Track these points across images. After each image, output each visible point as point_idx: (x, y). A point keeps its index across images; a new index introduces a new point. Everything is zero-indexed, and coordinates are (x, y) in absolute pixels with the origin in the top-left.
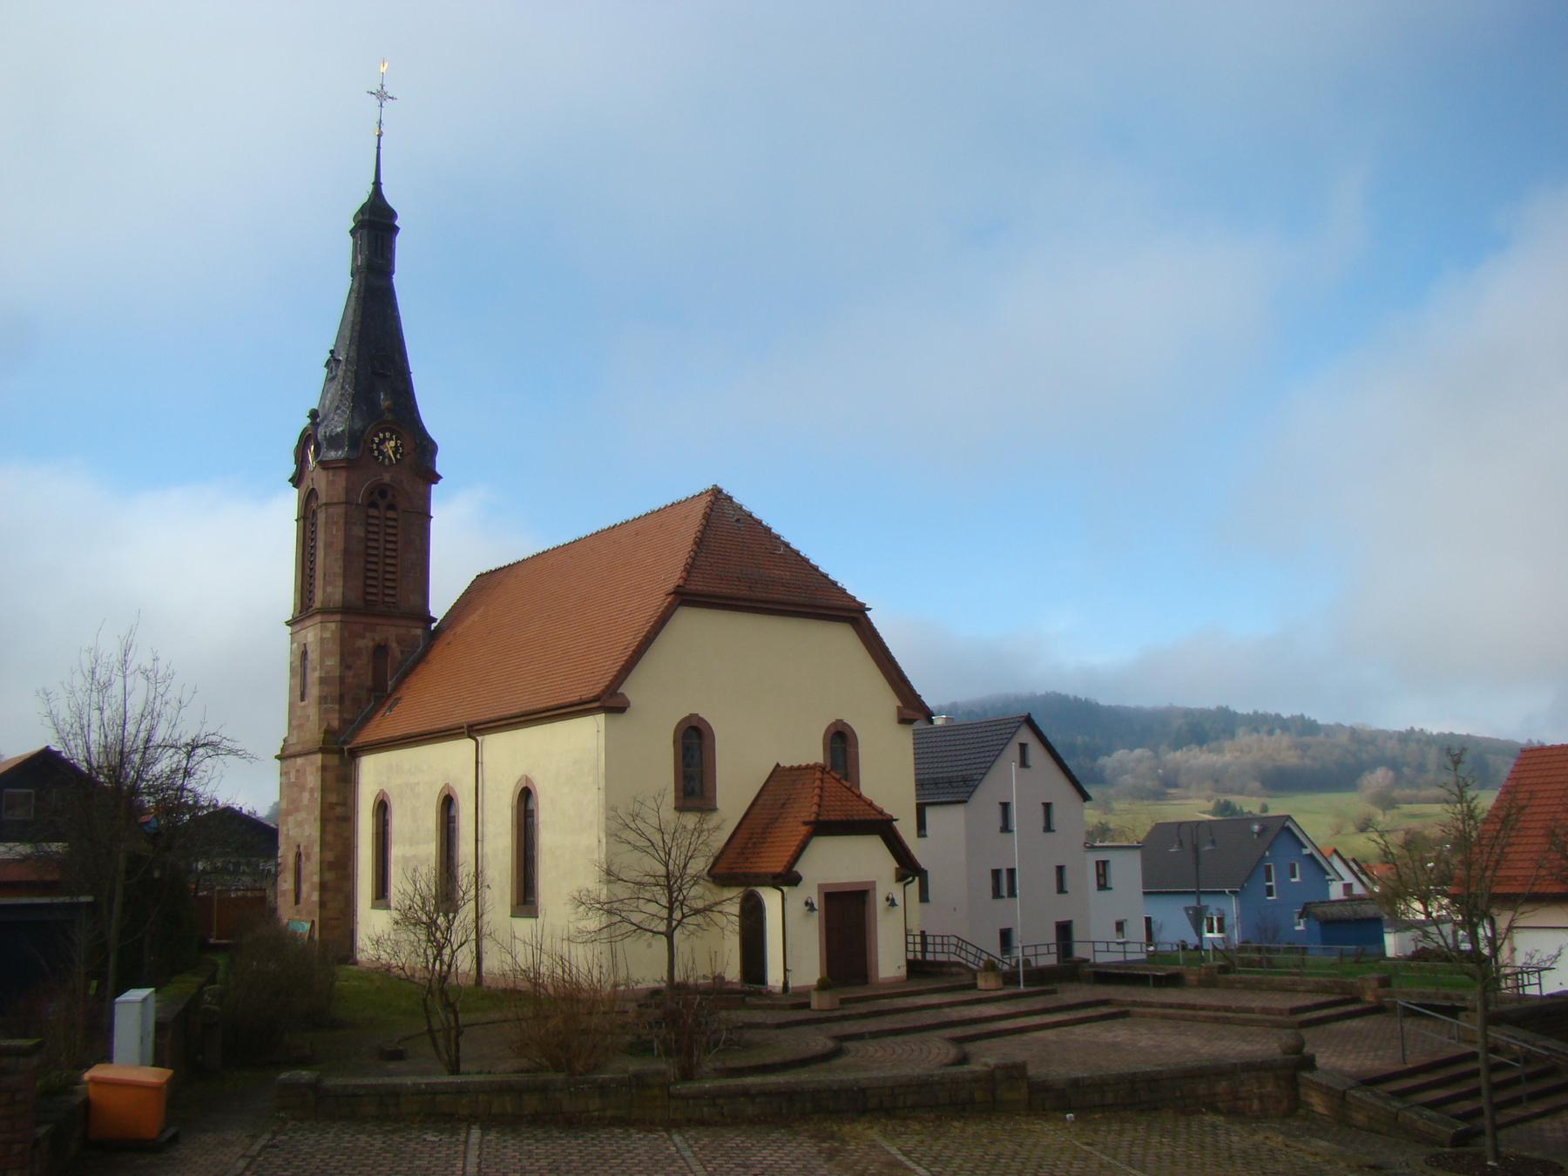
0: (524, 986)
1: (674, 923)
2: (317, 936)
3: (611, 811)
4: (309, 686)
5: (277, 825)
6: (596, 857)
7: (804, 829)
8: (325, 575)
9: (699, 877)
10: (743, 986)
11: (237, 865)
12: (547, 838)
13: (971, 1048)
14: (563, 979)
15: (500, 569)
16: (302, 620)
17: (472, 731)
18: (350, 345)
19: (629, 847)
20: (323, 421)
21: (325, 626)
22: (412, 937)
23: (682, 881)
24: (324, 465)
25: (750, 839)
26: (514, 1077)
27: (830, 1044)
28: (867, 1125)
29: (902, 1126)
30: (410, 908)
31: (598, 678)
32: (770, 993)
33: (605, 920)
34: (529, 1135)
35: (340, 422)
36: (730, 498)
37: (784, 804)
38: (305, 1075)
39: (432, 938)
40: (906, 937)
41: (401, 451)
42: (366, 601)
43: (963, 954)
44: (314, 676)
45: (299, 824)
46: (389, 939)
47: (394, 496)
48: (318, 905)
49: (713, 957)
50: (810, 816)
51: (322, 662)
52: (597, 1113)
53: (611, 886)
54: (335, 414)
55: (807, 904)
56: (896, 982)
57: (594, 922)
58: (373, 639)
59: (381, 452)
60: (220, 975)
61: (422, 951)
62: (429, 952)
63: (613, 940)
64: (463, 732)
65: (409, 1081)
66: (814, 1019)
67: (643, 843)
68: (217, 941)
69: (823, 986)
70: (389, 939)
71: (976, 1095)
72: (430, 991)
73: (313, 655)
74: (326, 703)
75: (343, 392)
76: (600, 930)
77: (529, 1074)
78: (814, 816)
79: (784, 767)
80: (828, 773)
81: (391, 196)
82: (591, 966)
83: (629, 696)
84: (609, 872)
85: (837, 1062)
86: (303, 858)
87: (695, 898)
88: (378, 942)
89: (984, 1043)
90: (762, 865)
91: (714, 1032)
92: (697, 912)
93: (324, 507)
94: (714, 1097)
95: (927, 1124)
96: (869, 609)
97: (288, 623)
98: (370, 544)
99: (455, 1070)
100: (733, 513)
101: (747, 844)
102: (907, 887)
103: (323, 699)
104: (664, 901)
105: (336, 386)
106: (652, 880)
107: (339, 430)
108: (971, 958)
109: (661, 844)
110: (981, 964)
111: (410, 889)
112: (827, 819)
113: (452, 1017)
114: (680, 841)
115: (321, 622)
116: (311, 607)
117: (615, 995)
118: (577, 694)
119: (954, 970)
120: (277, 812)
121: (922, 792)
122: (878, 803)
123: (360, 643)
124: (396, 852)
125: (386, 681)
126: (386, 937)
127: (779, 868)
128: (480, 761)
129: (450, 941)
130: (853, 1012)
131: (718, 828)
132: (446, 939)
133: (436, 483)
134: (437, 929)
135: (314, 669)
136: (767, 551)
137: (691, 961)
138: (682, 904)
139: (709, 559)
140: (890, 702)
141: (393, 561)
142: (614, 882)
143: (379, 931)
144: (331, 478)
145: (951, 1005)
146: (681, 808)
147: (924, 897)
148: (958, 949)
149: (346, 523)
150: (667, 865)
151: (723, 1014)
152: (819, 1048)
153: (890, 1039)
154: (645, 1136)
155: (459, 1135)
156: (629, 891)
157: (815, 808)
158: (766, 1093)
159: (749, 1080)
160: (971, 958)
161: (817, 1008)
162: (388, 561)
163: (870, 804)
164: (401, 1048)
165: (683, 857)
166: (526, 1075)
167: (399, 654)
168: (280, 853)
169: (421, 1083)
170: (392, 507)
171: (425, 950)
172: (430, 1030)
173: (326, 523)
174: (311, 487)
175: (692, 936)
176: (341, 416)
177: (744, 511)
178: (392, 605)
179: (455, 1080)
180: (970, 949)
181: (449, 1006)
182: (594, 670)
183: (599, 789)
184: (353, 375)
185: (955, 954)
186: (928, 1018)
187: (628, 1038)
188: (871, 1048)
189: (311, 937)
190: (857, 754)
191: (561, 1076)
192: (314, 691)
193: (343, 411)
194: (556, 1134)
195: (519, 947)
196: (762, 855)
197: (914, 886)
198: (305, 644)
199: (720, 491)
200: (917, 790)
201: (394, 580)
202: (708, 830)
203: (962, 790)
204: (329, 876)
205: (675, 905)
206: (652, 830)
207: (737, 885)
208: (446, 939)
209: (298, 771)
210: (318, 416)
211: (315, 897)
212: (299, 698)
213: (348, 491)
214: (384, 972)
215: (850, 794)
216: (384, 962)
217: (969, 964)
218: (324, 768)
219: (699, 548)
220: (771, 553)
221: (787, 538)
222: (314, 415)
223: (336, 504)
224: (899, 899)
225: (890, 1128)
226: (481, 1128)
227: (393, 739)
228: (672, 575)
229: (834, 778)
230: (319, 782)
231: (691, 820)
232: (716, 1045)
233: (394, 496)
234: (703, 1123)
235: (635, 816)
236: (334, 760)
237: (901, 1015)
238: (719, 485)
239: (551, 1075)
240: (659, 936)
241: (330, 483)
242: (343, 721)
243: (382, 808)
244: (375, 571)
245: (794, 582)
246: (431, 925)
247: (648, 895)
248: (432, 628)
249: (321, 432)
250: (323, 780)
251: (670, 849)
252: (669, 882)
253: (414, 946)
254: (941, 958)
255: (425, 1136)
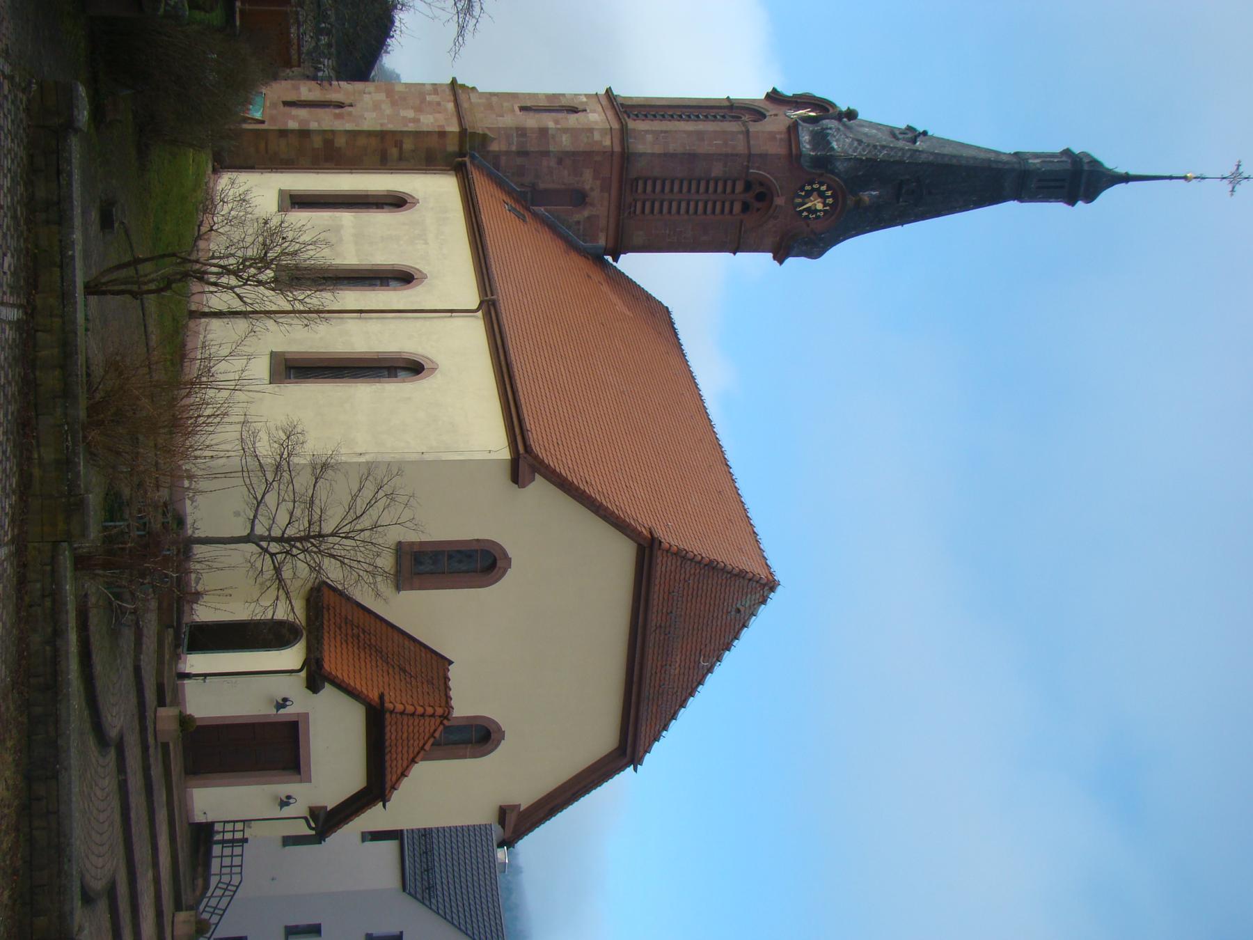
0: (192, 370)
1: (264, 544)
2: (246, 126)
3: (396, 469)
4: (537, 116)
5: (374, 81)
6: (343, 451)
7: (374, 695)
8: (666, 132)
9: (319, 572)
10: (186, 624)
11: (328, 33)
12: (363, 393)
13: (102, 905)
14: (199, 416)
15: (676, 334)
16: (613, 106)
17: (488, 306)
18: (932, 153)
19: (355, 490)
20: (845, 125)
21: (606, 134)
22: (249, 240)
23: (315, 553)
24: (793, 128)
25: (364, 632)
26: (81, 359)
27: (113, 733)
28: (10, 782)
29: (8, 826)
30: (284, 238)
31: (553, 451)
32: (177, 657)
33: (268, 461)
34: (10, 376)
35: (844, 145)
36: (764, 602)
37: (405, 671)
38: (83, 116)
39: (247, 263)
40: (231, 822)
41: (810, 216)
42: (637, 180)
43: (219, 892)
44: (549, 121)
45: (377, 107)
46: (247, 213)
47: (758, 210)
48: (282, 128)
49: (226, 592)
50: (391, 702)
51: (565, 130)
52: (36, 456)
53: (309, 470)
54: (853, 139)
55: (285, 700)
56: (186, 809)
57: (265, 448)
58: (592, 189)
59: (809, 194)
60: (199, 15)
61: (232, 252)
62: (232, 261)
63: (245, 474)
64: (487, 296)
65: (77, 236)
66: (145, 711)
67: (360, 505)
68: (238, 10)
69: (185, 721)
70: (247, 213)
71: (42, 918)
72: (186, 261)
73: (572, 120)
74: (518, 136)
75: (879, 148)
76: (256, 456)
77: (84, 376)
78: (391, 706)
79: (449, 670)
80: (441, 723)
81: (1110, 196)
82: (216, 447)
83: (532, 486)
84: (325, 466)
85: (91, 741)
86: (337, 111)
87: (294, 568)
88: (243, 200)
89: (106, 924)
90: (332, 645)
91: (132, 594)
92: (278, 570)
93: (743, 129)
94: (55, 595)
95: (8, 857)
96: (635, 770)
97: (609, 91)
98: (703, 184)
99: (91, 289)
100: (747, 605)
101: (358, 627)
102: (303, 821)
103: (522, 132)
104: (291, 532)
105: (885, 139)
106: (316, 517)
107: (834, 145)
108: (213, 902)
109: (358, 527)
110: (206, 916)
111: (305, 238)
112: (387, 722)
113: (153, 286)
114: (362, 549)
115: (611, 128)
116: (629, 117)
117: (176, 476)
118: (533, 426)
119: (200, 882)
120: (390, 80)
121: (416, 836)
122: (405, 782)
123: (588, 175)
124: (346, 218)
125: (544, 205)
126: (249, 210)
127: (328, 666)
128: (454, 314)
129: (245, 284)
130: (152, 760)
131: (378, 595)
132: (248, 280)
133: (775, 258)
134: (259, 269)
135: (557, 122)
136: (703, 647)
137: (220, 566)
138: (287, 553)
139: (691, 578)
140: (525, 796)
141: (683, 210)
142: (313, 474)
143: (254, 202)
144: (778, 136)
145: (157, 880)
146: (400, 548)
147: (289, 841)
148: (230, 888)
149: (727, 155)
150: (333, 534)
151: (153, 604)
152: (109, 718)
153: (116, 804)
154: (7, 514)
155: (12, 294)
156: (303, 490)
157: (399, 707)
158: (55, 660)
159: (73, 637)
160: (213, 902)
161: (158, 714)
162: (683, 205)
163: (403, 774)
164: (116, 225)
165: (343, 553)
166: (85, 373)
167: (575, 220)
168: (343, 84)
169: (74, 252)
170: (746, 207)
171: (233, 255)
172: (136, 262)
173: (724, 132)
174: (767, 114)
175: (249, 564)
176: (850, 145)
177: (749, 619)
178: (632, 209)
179: (78, 290)
180: (225, 900)
181: (167, 283)
182: (561, 446)
183: (423, 453)
184: (898, 159)
185: (220, 882)
186: (142, 852)
187: (127, 492)
188: (108, 783)
189: (246, 120)
190: (464, 757)
191: (82, 414)
192: (531, 121)
193: (856, 148)
194: (11, 408)
195: (238, 364)
196: (344, 646)
197: (303, 829)
198: (585, 110)
199: (772, 589)
200: (419, 830)
201: (661, 212)
202: (375, 583)
203: (419, 884)
204: (317, 142)
205: (286, 545)
206: (375, 518)
207: (308, 618)
208: (248, 280)
209: (439, 104)
210: (850, 119)
211: (293, 125)
212: (524, 105)
213: (764, 156)
214: (208, 204)
215: (416, 750)
216: (219, 207)
217: (205, 900)
218: (442, 134)
219: (706, 565)
220: (701, 650)
221: (719, 669)
222: (851, 115)
223: (748, 142)
224: (287, 811)
225: (6, 811)
226: (18, 320)
227: (478, 213)
228: (669, 538)
229: (435, 731)
230: (425, 129)
231: (386, 562)
232: (118, 596)
233: (758, 210)
234: (22, 582)
235: (391, 496)
236: (452, 146)
237: (147, 818)
238: (779, 589)
239: (83, 403)
240: (249, 526)
241: (772, 136)
242: (497, 156)
243: (398, 202)
244: (672, 190)
245: (667, 679)
246: (263, 262)
247: (298, 512)
248: (606, 257)
249: (831, 124)
250: (429, 133)
251: (352, 538)
252: (314, 537)
253: (238, 242)
254: (215, 865)
255: (9, 255)
